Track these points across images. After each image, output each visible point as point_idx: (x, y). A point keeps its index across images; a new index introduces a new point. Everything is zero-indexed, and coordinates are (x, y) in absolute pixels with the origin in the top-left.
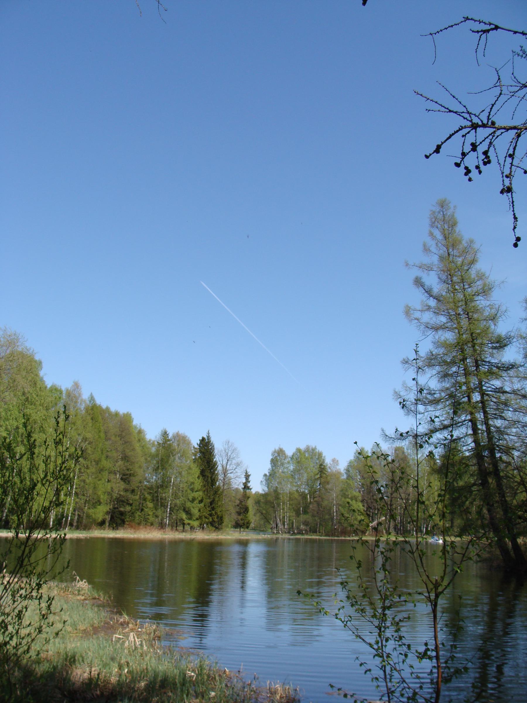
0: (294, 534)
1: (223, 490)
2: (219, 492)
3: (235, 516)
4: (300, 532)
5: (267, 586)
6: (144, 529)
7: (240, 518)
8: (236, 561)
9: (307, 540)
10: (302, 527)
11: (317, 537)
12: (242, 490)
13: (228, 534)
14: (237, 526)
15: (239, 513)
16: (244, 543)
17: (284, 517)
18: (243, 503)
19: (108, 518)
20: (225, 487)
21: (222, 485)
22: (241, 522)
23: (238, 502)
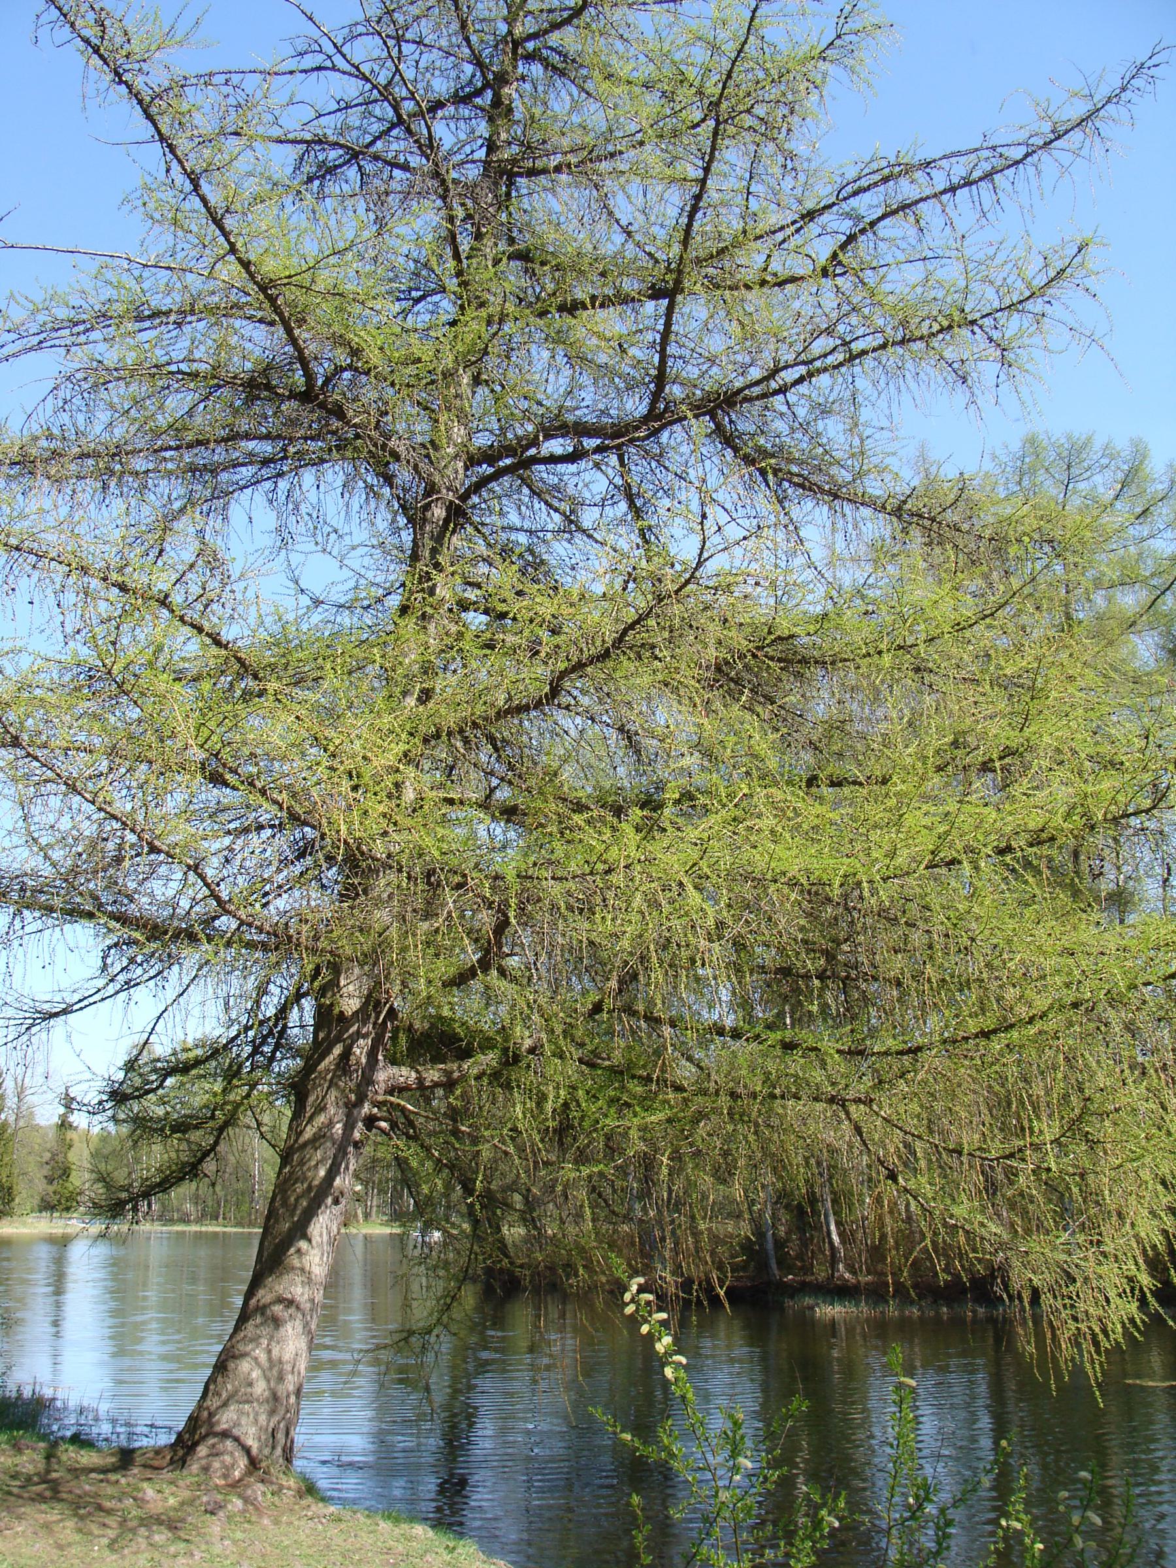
0: (172, 1221)
1: (16, 1131)
2: (6, 1135)
3: (41, 1186)
4: (185, 1220)
5: (112, 1343)
6: (107, 1332)
7: (51, 1189)
8: (41, 1289)
9: (199, 1236)
10: (188, 1206)
11: (218, 1229)
12: (52, 1134)
13: (24, 1224)
14: (47, 1206)
15: (50, 1180)
16: (62, 1243)
17: (990, 1086)
18: (60, 1158)
19: (652, 1454)
20: (21, 1123)
21: (12, 1119)
22: (54, 1200)
23: (48, 1156)
